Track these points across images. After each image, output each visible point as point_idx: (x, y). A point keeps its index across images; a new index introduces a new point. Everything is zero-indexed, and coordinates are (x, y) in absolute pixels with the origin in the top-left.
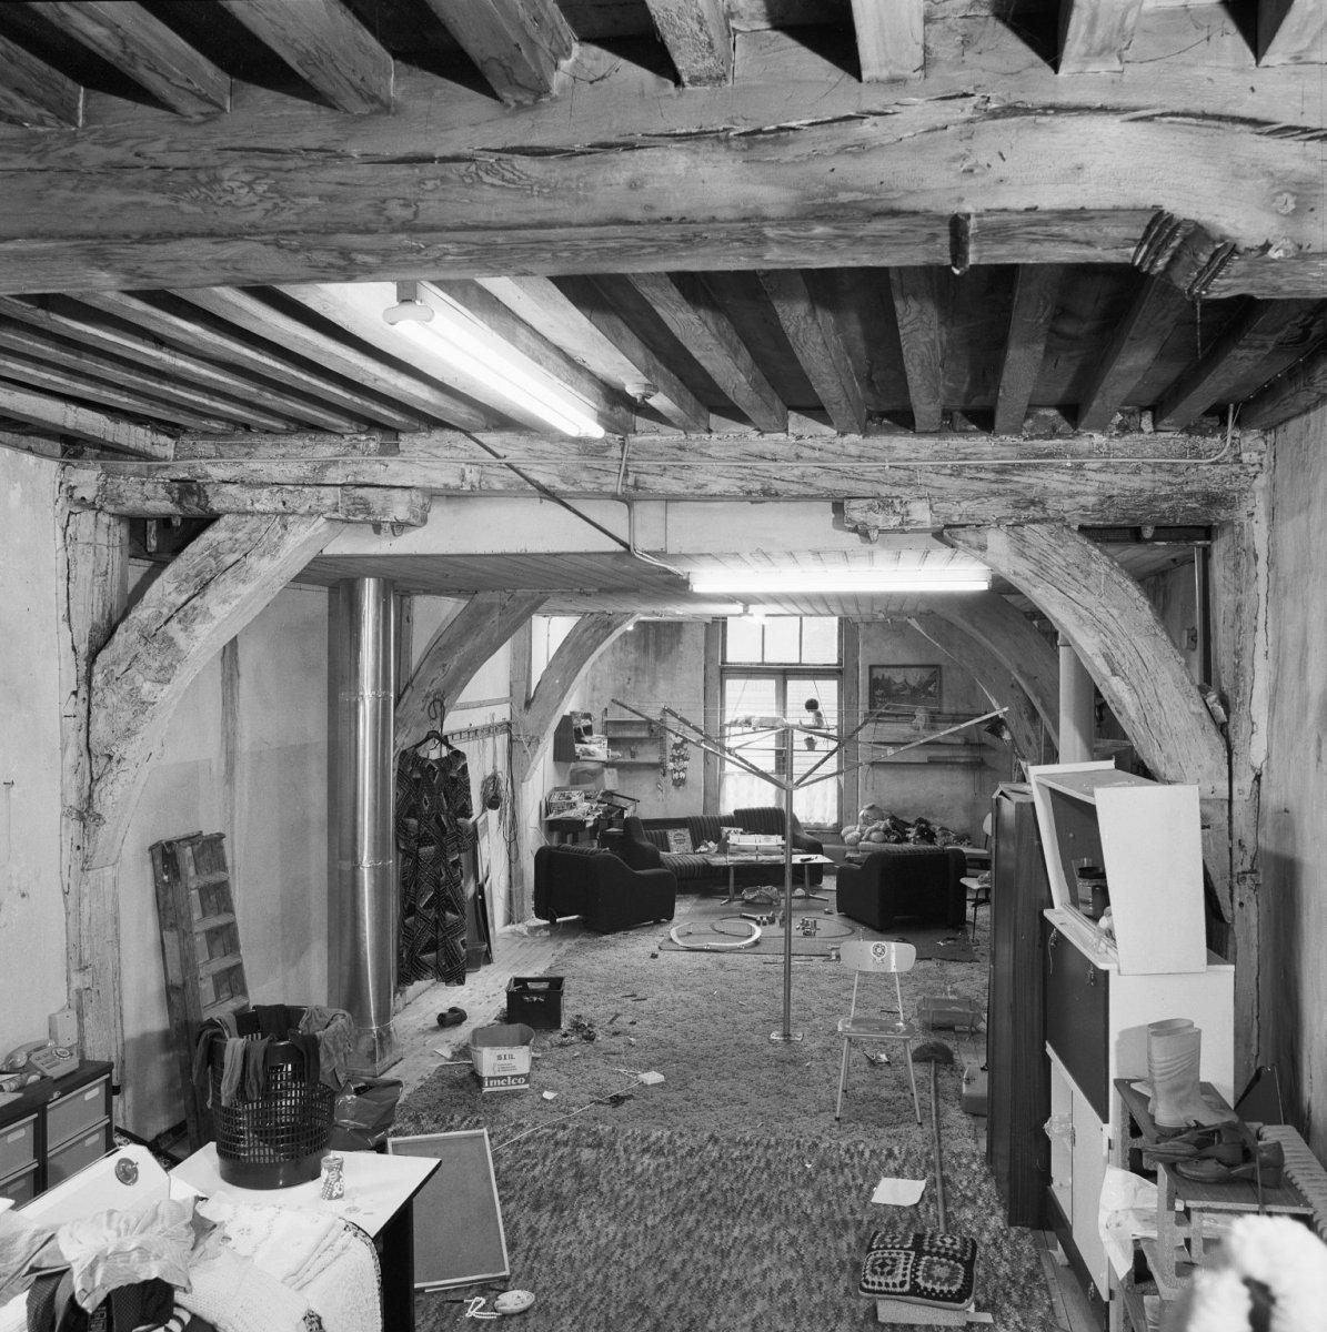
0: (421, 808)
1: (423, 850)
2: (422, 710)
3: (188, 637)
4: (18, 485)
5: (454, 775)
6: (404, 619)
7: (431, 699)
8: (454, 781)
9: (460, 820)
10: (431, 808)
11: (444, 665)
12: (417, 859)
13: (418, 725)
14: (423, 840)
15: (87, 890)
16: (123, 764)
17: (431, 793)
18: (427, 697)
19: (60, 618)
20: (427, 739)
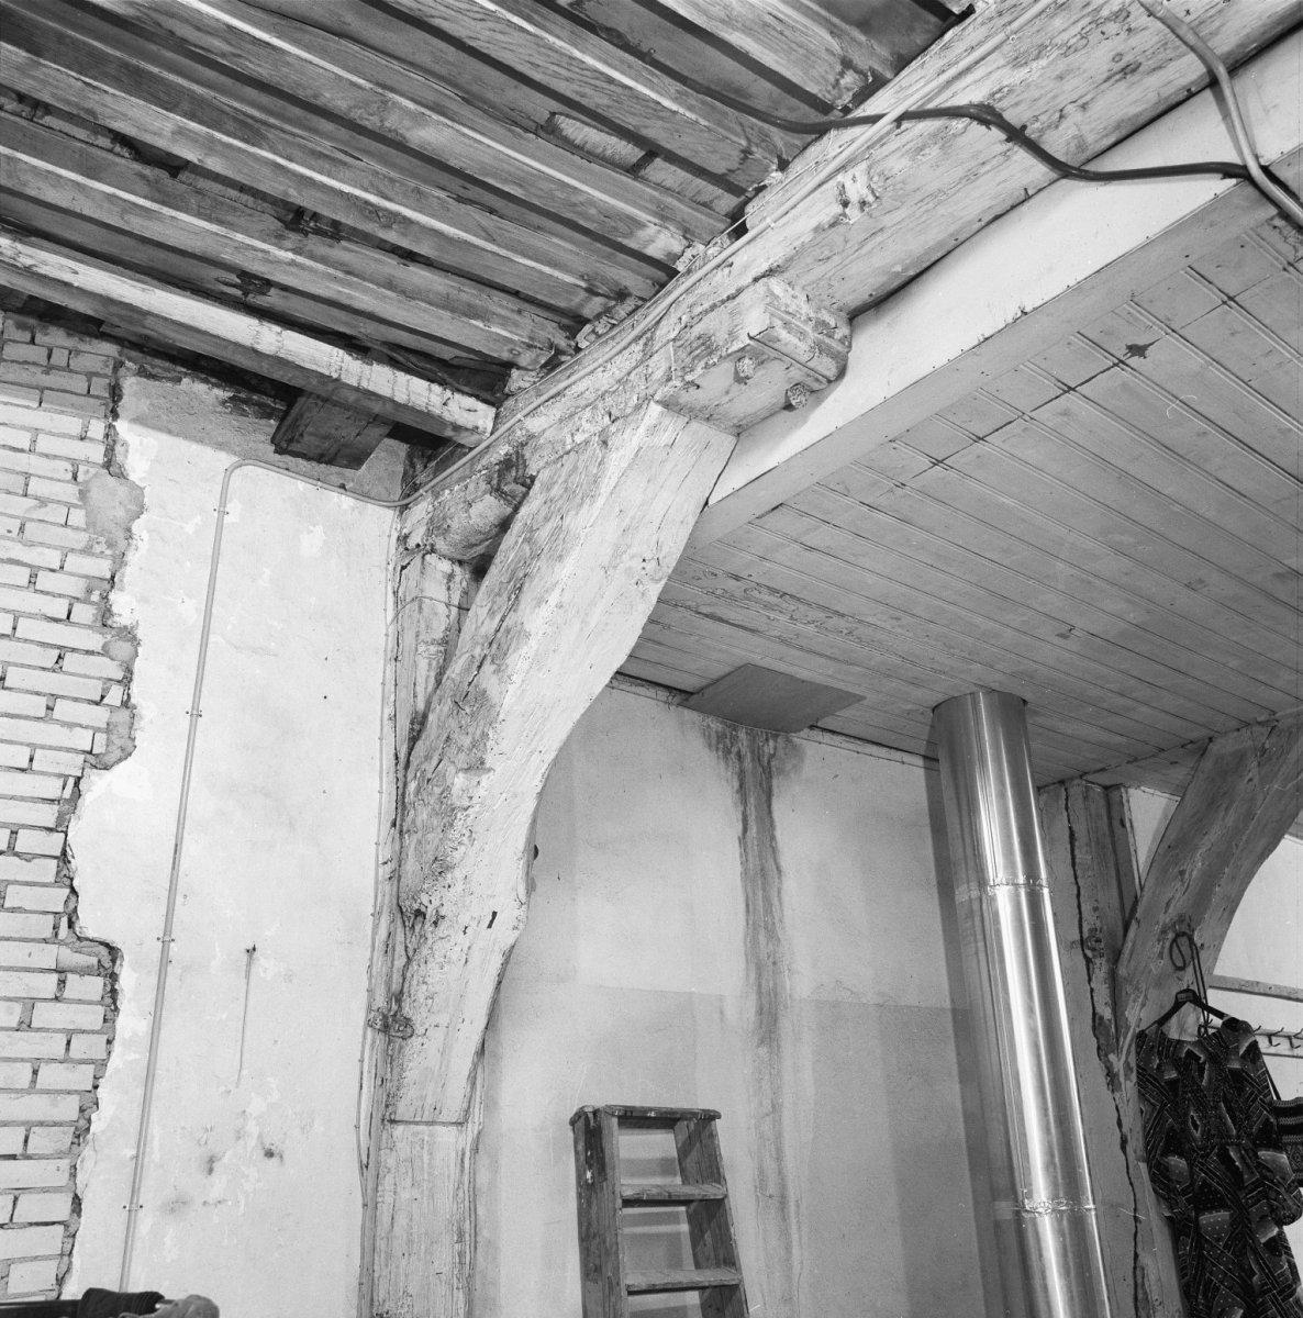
0: (1189, 1138)
1: (1207, 1219)
2: (1161, 955)
3: (501, 681)
4: (319, 529)
5: (1236, 1066)
6: (1116, 823)
7: (1171, 936)
8: (1238, 1078)
9: (1264, 1154)
10: (1207, 1135)
11: (1182, 873)
12: (1200, 1240)
13: (1159, 984)
14: (1205, 1199)
15: (391, 1162)
16: (443, 925)
17: (1201, 1107)
18: (1164, 932)
19: (386, 716)
20: (1177, 1006)
